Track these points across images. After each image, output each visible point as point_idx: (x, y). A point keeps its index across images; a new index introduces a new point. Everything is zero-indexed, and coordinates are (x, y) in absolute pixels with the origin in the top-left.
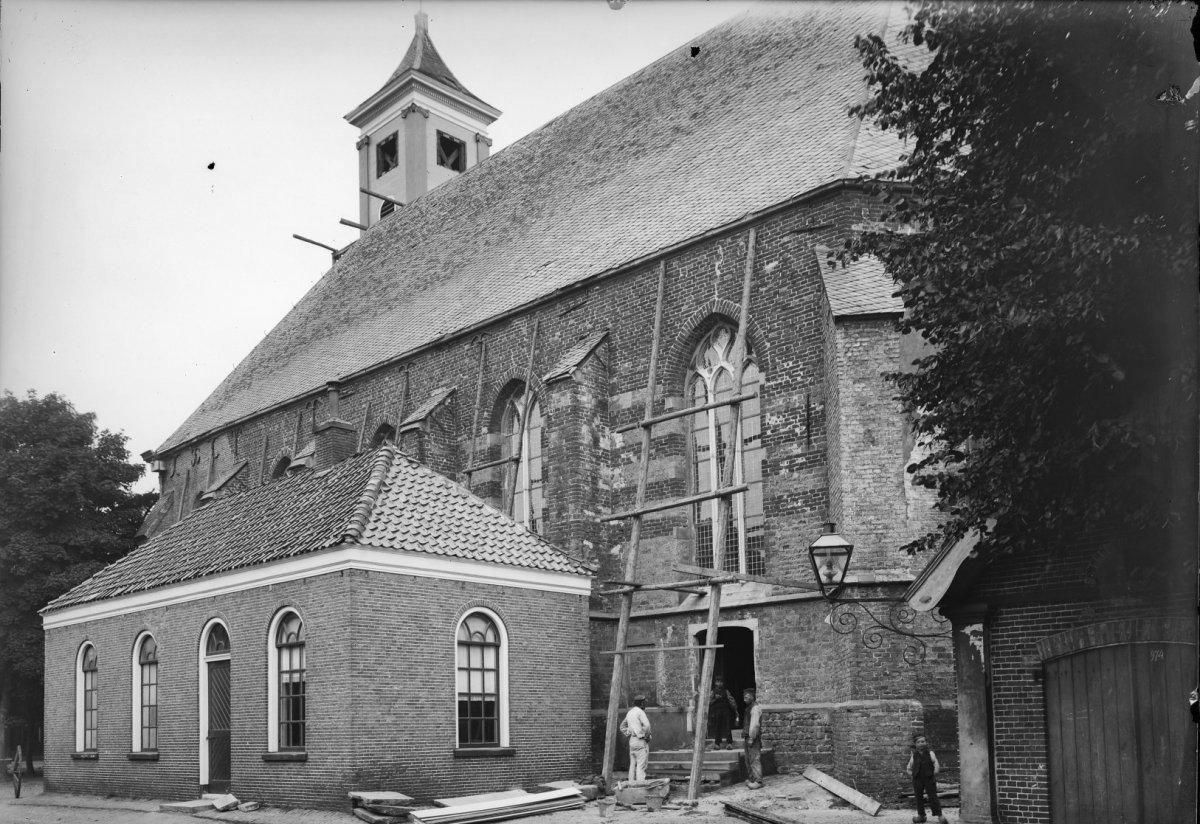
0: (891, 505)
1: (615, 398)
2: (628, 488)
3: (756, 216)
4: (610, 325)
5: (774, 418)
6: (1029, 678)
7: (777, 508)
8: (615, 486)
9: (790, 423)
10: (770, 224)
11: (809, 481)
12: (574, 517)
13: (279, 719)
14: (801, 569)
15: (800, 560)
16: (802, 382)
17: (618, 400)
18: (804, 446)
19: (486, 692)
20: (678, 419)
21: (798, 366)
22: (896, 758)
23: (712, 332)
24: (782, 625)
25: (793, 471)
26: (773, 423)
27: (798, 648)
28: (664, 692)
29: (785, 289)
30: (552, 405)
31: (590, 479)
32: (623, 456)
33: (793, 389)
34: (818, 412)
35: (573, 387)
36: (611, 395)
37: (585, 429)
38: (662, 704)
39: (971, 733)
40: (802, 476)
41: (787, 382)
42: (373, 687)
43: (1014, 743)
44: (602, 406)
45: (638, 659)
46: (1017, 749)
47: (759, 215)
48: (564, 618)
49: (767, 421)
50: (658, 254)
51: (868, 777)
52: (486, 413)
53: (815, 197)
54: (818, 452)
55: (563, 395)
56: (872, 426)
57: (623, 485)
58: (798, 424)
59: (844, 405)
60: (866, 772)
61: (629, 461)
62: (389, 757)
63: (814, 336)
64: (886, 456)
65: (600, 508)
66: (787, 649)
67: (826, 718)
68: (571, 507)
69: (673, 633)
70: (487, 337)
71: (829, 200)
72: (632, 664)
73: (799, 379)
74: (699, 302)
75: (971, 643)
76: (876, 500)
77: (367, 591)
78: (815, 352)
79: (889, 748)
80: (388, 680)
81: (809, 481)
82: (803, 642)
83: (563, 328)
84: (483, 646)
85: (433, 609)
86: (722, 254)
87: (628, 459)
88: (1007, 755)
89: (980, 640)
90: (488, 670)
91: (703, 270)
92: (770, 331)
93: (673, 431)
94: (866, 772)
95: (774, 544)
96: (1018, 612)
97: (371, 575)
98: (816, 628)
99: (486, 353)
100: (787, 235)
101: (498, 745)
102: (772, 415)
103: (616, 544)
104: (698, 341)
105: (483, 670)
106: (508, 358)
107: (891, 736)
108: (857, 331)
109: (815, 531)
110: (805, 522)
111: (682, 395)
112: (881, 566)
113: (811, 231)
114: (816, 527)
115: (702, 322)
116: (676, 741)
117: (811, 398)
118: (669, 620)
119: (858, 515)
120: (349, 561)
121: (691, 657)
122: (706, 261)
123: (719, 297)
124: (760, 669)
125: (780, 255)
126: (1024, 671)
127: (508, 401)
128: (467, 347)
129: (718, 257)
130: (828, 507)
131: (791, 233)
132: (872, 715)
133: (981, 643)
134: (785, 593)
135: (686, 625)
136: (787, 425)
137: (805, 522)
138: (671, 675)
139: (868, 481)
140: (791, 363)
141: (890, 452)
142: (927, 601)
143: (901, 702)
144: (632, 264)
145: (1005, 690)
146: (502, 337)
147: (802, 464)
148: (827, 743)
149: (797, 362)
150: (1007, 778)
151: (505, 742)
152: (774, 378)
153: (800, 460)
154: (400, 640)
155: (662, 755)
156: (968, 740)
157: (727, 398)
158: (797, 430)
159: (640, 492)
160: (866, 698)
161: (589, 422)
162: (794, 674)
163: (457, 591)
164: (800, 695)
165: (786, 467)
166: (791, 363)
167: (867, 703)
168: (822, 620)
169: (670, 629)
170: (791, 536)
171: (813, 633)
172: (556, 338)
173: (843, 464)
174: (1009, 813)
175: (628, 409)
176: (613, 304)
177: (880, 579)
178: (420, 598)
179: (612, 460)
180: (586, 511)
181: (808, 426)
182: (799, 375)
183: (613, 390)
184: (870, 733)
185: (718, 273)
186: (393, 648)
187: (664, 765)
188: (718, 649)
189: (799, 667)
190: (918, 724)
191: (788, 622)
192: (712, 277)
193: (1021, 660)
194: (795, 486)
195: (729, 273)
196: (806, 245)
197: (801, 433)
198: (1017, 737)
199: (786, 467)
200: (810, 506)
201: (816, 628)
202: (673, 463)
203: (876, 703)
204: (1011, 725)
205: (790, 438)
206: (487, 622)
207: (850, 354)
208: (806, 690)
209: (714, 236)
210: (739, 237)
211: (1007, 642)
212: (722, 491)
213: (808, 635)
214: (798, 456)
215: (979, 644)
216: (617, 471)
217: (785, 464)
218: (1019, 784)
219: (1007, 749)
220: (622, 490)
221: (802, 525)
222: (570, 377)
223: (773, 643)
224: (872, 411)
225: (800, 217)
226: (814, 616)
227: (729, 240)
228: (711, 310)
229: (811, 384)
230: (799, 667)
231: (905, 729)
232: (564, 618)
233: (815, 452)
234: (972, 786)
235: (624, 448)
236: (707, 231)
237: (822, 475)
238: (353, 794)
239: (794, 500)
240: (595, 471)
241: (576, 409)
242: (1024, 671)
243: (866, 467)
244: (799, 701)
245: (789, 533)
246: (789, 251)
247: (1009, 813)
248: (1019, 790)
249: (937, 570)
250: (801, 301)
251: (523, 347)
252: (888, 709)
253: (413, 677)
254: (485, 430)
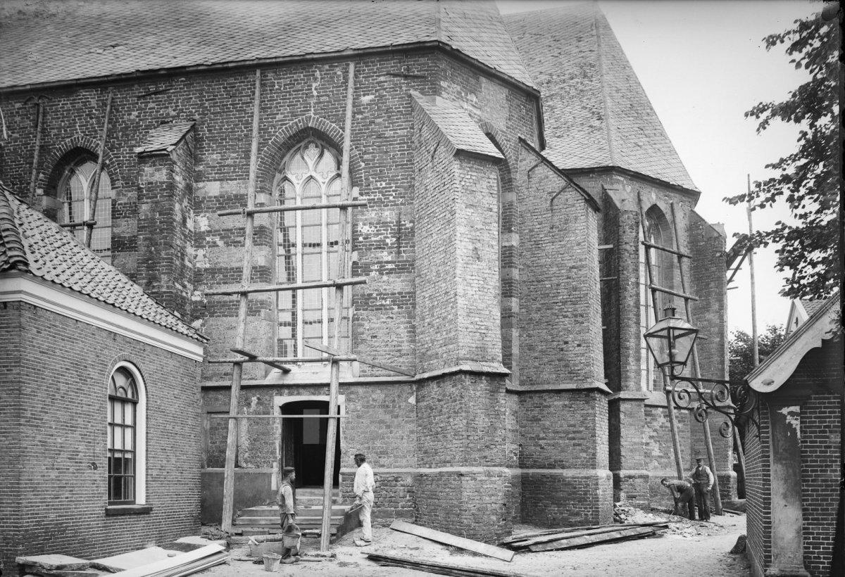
0: (490, 311)
1: (201, 185)
2: (212, 269)
3: (356, 52)
4: (197, 117)
5: (367, 227)
6: (835, 452)
7: (367, 304)
8: (198, 265)
9: (382, 234)
10: (368, 62)
11: (397, 284)
12: (168, 287)
13: (135, 480)
14: (388, 356)
15: (387, 349)
16: (394, 201)
17: (204, 187)
18: (394, 255)
19: (116, 448)
20: (267, 214)
21: (391, 187)
22: (493, 514)
23: (302, 144)
24: (368, 402)
25: (383, 274)
26: (366, 231)
27: (382, 422)
28: (247, 455)
29: (380, 120)
30: (144, 178)
31: (179, 254)
32: (208, 239)
33: (385, 206)
34: (407, 229)
35: (170, 164)
36: (196, 181)
37: (177, 206)
38: (245, 465)
39: (785, 496)
40: (391, 280)
41: (381, 199)
42: (39, 438)
43: (820, 505)
44: (189, 189)
45: (219, 424)
46: (822, 510)
47: (360, 52)
48: (185, 381)
49: (359, 229)
50: (255, 62)
51: (474, 529)
52: (41, 175)
53: (412, 50)
54: (407, 261)
55: (158, 170)
56: (478, 245)
57: (208, 266)
58: (389, 236)
59: (459, 224)
60: (473, 525)
61: (215, 245)
62: (52, 516)
63: (407, 165)
64: (487, 271)
65: (186, 283)
66: (371, 422)
67: (409, 480)
68: (164, 278)
69: (258, 403)
70: (46, 100)
71: (423, 56)
72: (211, 428)
73: (391, 198)
74: (294, 115)
75: (787, 421)
76: (481, 306)
77: (35, 330)
78: (407, 179)
79: (489, 505)
80: (53, 431)
81: (397, 284)
82: (387, 417)
83: (140, 109)
84: (124, 401)
85: (91, 358)
86: (319, 77)
87: (215, 243)
88: (812, 514)
89: (796, 419)
90: (128, 426)
91: (299, 87)
92: (365, 153)
93: (264, 223)
94: (473, 525)
95: (363, 334)
96: (825, 398)
97: (40, 313)
98: (400, 407)
99: (44, 116)
100: (384, 75)
101: (134, 502)
102: (364, 224)
103: (197, 318)
104: (289, 149)
105: (123, 426)
106: (72, 125)
107: (491, 496)
108: (469, 165)
109: (402, 326)
110: (392, 318)
111: (271, 194)
112: (484, 359)
113: (406, 77)
114: (402, 323)
115: (297, 133)
116: (260, 499)
117: (402, 216)
118: (254, 391)
119: (468, 316)
120: (20, 292)
121: (276, 425)
122: (304, 80)
123: (315, 114)
124: (346, 438)
125: (376, 91)
126: (830, 447)
127: (68, 168)
128: (18, 105)
129: (315, 79)
130: (414, 308)
131: (387, 74)
132: (479, 479)
133: (798, 422)
134: (372, 376)
135: (271, 397)
136: (378, 235)
137: (392, 318)
138: (254, 440)
139: (474, 289)
140: (384, 184)
141: (490, 269)
142: (769, 384)
143: (497, 469)
144: (225, 65)
145: (812, 461)
146: (63, 103)
147: (391, 269)
148: (409, 501)
149: (390, 184)
150: (813, 534)
151: (141, 500)
152: (368, 193)
153: (390, 266)
154: (63, 387)
155: (263, 511)
156: (783, 502)
157: (338, 201)
158: (388, 241)
159: (246, 273)
160: (473, 465)
161: (181, 202)
162: (378, 443)
163: (110, 342)
164: (382, 461)
165: (376, 270)
166: (384, 184)
167: (475, 469)
168: (406, 401)
169: (254, 400)
170: (379, 328)
171: (397, 410)
172: (132, 117)
173: (458, 272)
174: (813, 563)
175: (215, 197)
176: (201, 96)
177: (486, 369)
178: (81, 345)
179: (195, 240)
180: (176, 284)
181: (398, 239)
182: (392, 195)
183: (199, 177)
184: (476, 494)
185: (315, 93)
186: (58, 396)
187: (271, 520)
188: (284, 419)
189: (383, 438)
190: (508, 487)
191: (373, 400)
192: (309, 96)
193: (828, 437)
194: (384, 287)
195: (326, 95)
196: (401, 88)
197: (392, 244)
198: (822, 500)
199: (376, 270)
200: (398, 305)
201: (400, 407)
202: (264, 253)
203: (480, 469)
204: (817, 490)
205: (381, 246)
206: (127, 378)
207: (463, 183)
208: (389, 457)
209: (313, 60)
210: (337, 66)
211: (815, 422)
212: (340, 281)
213: (392, 411)
214: (388, 262)
215: (796, 423)
216: (201, 252)
217: (376, 267)
218: (823, 539)
219: (812, 510)
220: (206, 270)
221: (390, 320)
222: (169, 155)
223: (358, 417)
224: (478, 233)
225: (396, 63)
226: (399, 396)
227: (327, 67)
228: (307, 124)
229: (402, 204)
230: (383, 438)
231: (500, 491)
232: (185, 381)
233: (405, 261)
234: (785, 540)
235: (209, 232)
236: (307, 54)
237: (410, 281)
238: (21, 559)
239: (383, 299)
240: (183, 248)
241: (171, 186)
242: (830, 447)
243: (474, 278)
244: (383, 466)
245: (377, 325)
246: (385, 89)
247: (813, 563)
248: (823, 544)
249: (780, 358)
250: (394, 133)
251: (91, 118)
252: (489, 475)
253: (73, 428)
254: (40, 191)
